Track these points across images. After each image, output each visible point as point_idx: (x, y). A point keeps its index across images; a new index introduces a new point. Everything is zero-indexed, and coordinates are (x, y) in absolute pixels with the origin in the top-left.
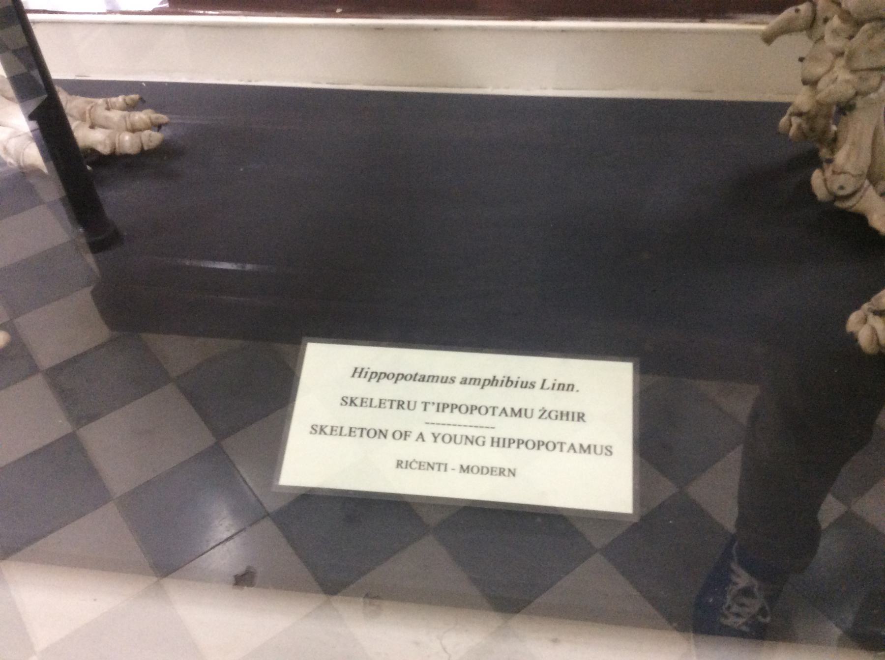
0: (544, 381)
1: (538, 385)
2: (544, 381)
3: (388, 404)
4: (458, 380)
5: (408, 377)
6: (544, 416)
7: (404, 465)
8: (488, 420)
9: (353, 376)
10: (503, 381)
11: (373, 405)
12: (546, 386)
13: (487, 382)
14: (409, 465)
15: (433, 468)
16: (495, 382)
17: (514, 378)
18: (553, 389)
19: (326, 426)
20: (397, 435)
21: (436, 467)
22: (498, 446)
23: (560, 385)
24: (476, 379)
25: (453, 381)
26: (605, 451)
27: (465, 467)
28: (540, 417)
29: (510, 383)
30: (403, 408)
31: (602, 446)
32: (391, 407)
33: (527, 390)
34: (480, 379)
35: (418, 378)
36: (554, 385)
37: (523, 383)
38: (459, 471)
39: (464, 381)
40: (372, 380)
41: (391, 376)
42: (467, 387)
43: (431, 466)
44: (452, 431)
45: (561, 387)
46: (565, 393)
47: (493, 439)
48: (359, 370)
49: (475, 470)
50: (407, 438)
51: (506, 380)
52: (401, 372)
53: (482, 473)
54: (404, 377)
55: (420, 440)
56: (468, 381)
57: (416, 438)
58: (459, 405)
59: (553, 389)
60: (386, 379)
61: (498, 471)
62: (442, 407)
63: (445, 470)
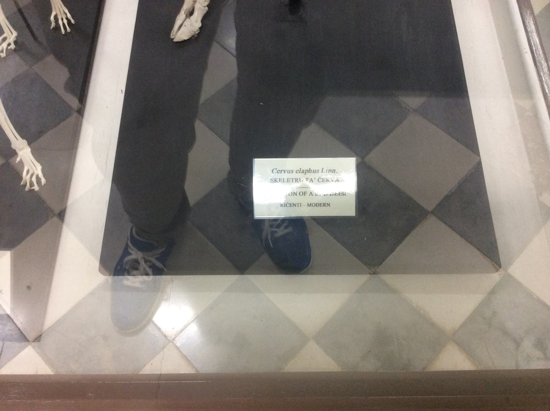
0: (323, 169)
2: (323, 169)
3: (291, 180)
11: (285, 181)
12: (324, 171)
13: (307, 171)
15: (295, 206)
16: (310, 171)
19: (277, 179)
20: (301, 194)
30: (298, 182)
32: (293, 182)
34: (313, 172)
38: (307, 206)
49: (314, 205)
50: (305, 194)
55: (311, 195)
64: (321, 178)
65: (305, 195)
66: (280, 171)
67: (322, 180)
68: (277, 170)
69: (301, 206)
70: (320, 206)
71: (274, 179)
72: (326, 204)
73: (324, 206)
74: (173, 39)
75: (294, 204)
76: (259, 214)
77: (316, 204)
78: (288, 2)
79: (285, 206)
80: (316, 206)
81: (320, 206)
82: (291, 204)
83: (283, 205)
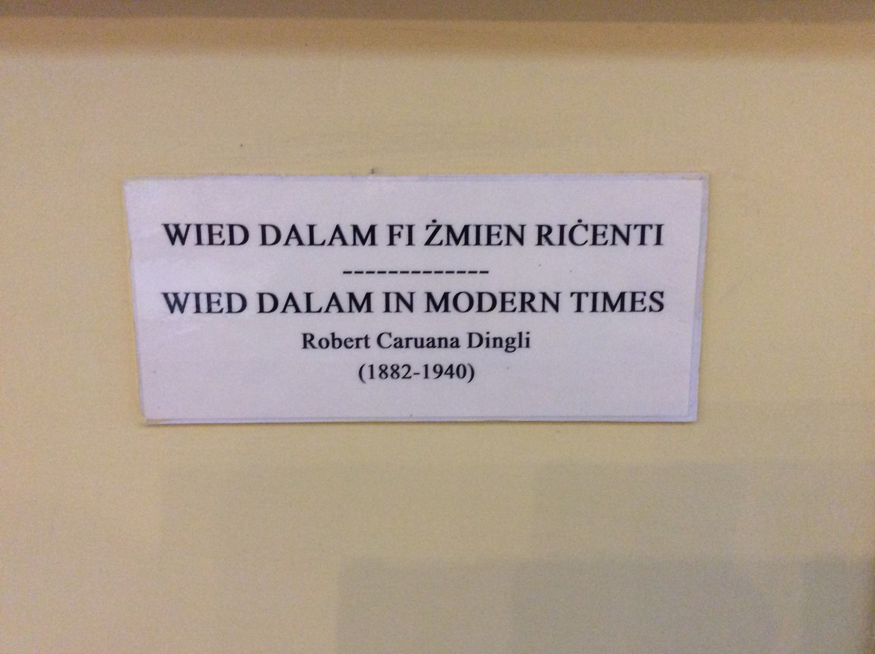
6: (436, 240)
7: (555, 237)
12: (405, 233)
14: (567, 235)
15: (626, 240)
21: (635, 235)
27: (438, 298)
28: (428, 243)
43: (621, 235)
49: (463, 302)
50: (396, 238)
53: (480, 309)
64: (586, 227)
66: (351, 340)
67: (589, 235)
68: (394, 336)
69: (658, 242)
70: (503, 309)
72: (538, 299)
73: (523, 310)
75: (616, 229)
76: (131, 189)
77: (480, 295)
79: (562, 243)
80: (480, 309)
81: (503, 309)
82: (600, 230)
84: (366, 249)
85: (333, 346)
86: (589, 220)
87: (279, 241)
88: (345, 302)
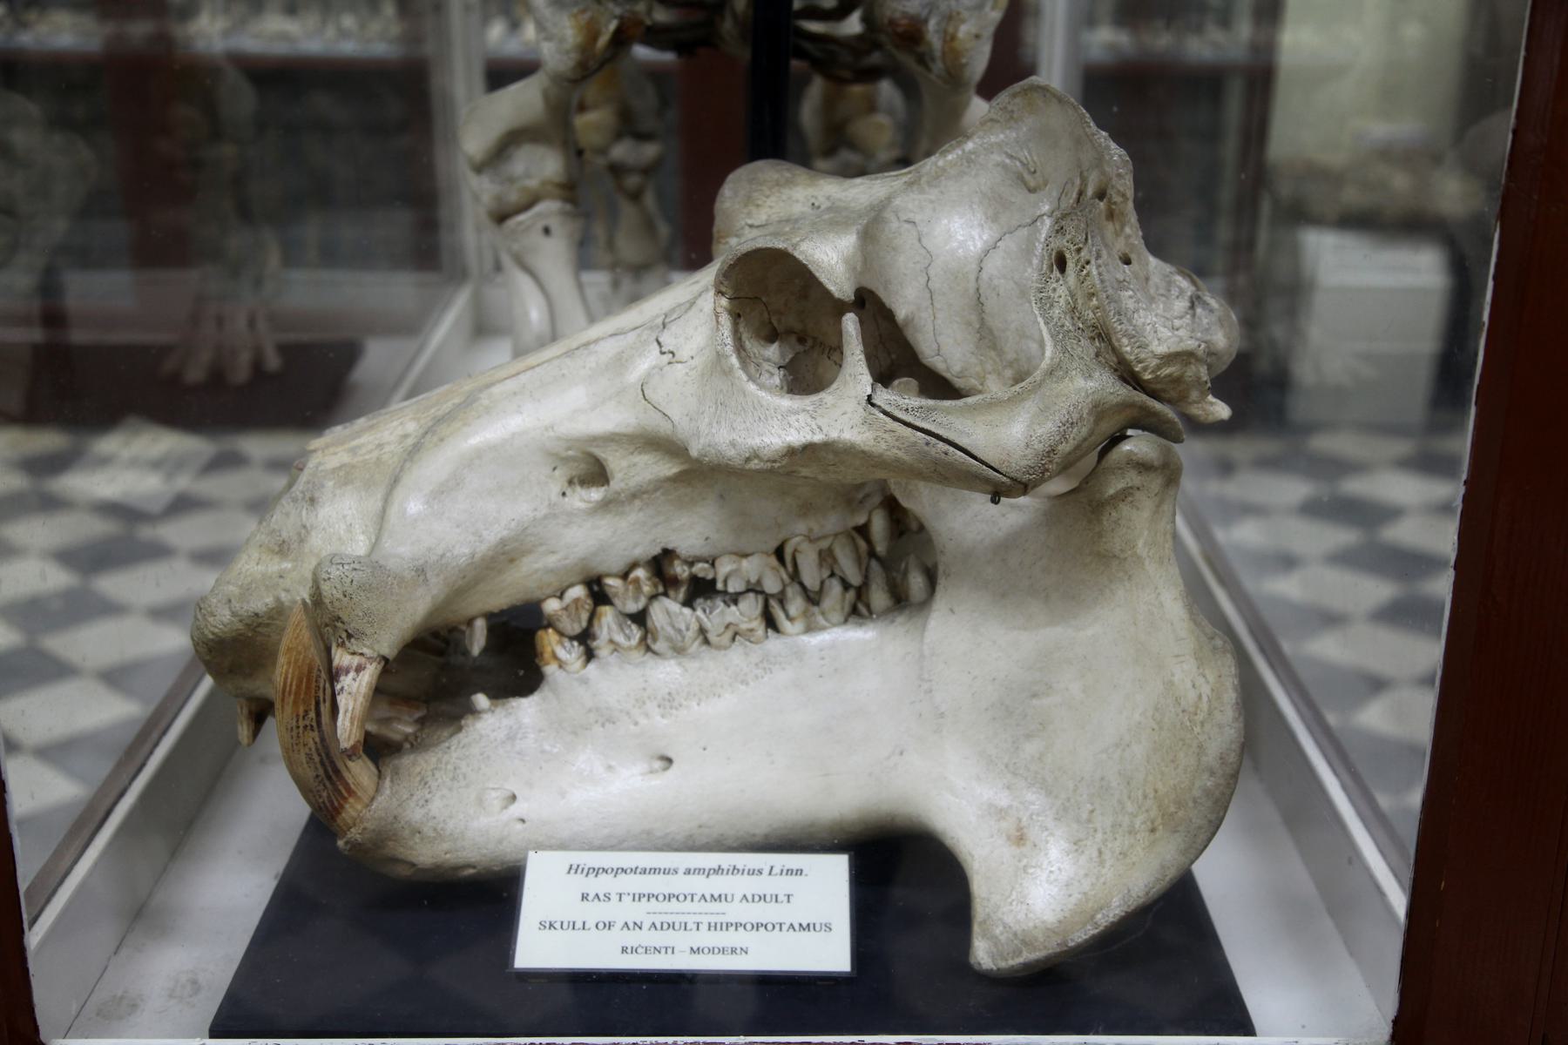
0: (772, 868)
1: (766, 871)
2: (772, 868)
4: (681, 871)
5: (629, 871)
7: (629, 951)
8: (687, 906)
9: (569, 872)
10: (728, 870)
12: (774, 872)
13: (712, 871)
15: (659, 952)
16: (720, 871)
17: (740, 867)
18: (781, 874)
19: (556, 922)
20: (601, 926)
21: (663, 951)
22: (716, 929)
23: (788, 870)
24: (700, 870)
25: (676, 872)
26: (824, 927)
29: (736, 871)
31: (821, 924)
33: (754, 877)
34: (704, 870)
35: (638, 871)
36: (782, 871)
37: (749, 870)
39: (688, 872)
40: (589, 876)
41: (610, 871)
42: (690, 877)
44: (670, 919)
45: (790, 872)
46: (794, 877)
47: (710, 924)
48: (574, 867)
49: (706, 951)
51: (731, 869)
52: (602, 866)
54: (624, 871)
56: (692, 871)
57: (621, 927)
58: (656, 894)
59: (781, 874)
60: (604, 873)
61: (730, 951)
62: (637, 897)
63: (673, 952)
65: (609, 928)
71: (548, 923)
74: (257, 365)
76: (983, 954)
78: (851, 248)
83: (555, 925)
84: (717, 903)
85: (713, 953)
86: (644, 944)
87: (805, 266)
88: (797, 927)
